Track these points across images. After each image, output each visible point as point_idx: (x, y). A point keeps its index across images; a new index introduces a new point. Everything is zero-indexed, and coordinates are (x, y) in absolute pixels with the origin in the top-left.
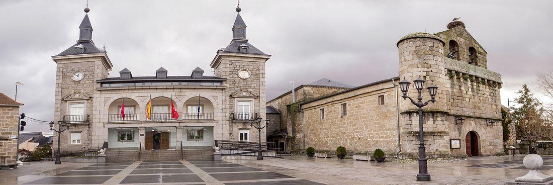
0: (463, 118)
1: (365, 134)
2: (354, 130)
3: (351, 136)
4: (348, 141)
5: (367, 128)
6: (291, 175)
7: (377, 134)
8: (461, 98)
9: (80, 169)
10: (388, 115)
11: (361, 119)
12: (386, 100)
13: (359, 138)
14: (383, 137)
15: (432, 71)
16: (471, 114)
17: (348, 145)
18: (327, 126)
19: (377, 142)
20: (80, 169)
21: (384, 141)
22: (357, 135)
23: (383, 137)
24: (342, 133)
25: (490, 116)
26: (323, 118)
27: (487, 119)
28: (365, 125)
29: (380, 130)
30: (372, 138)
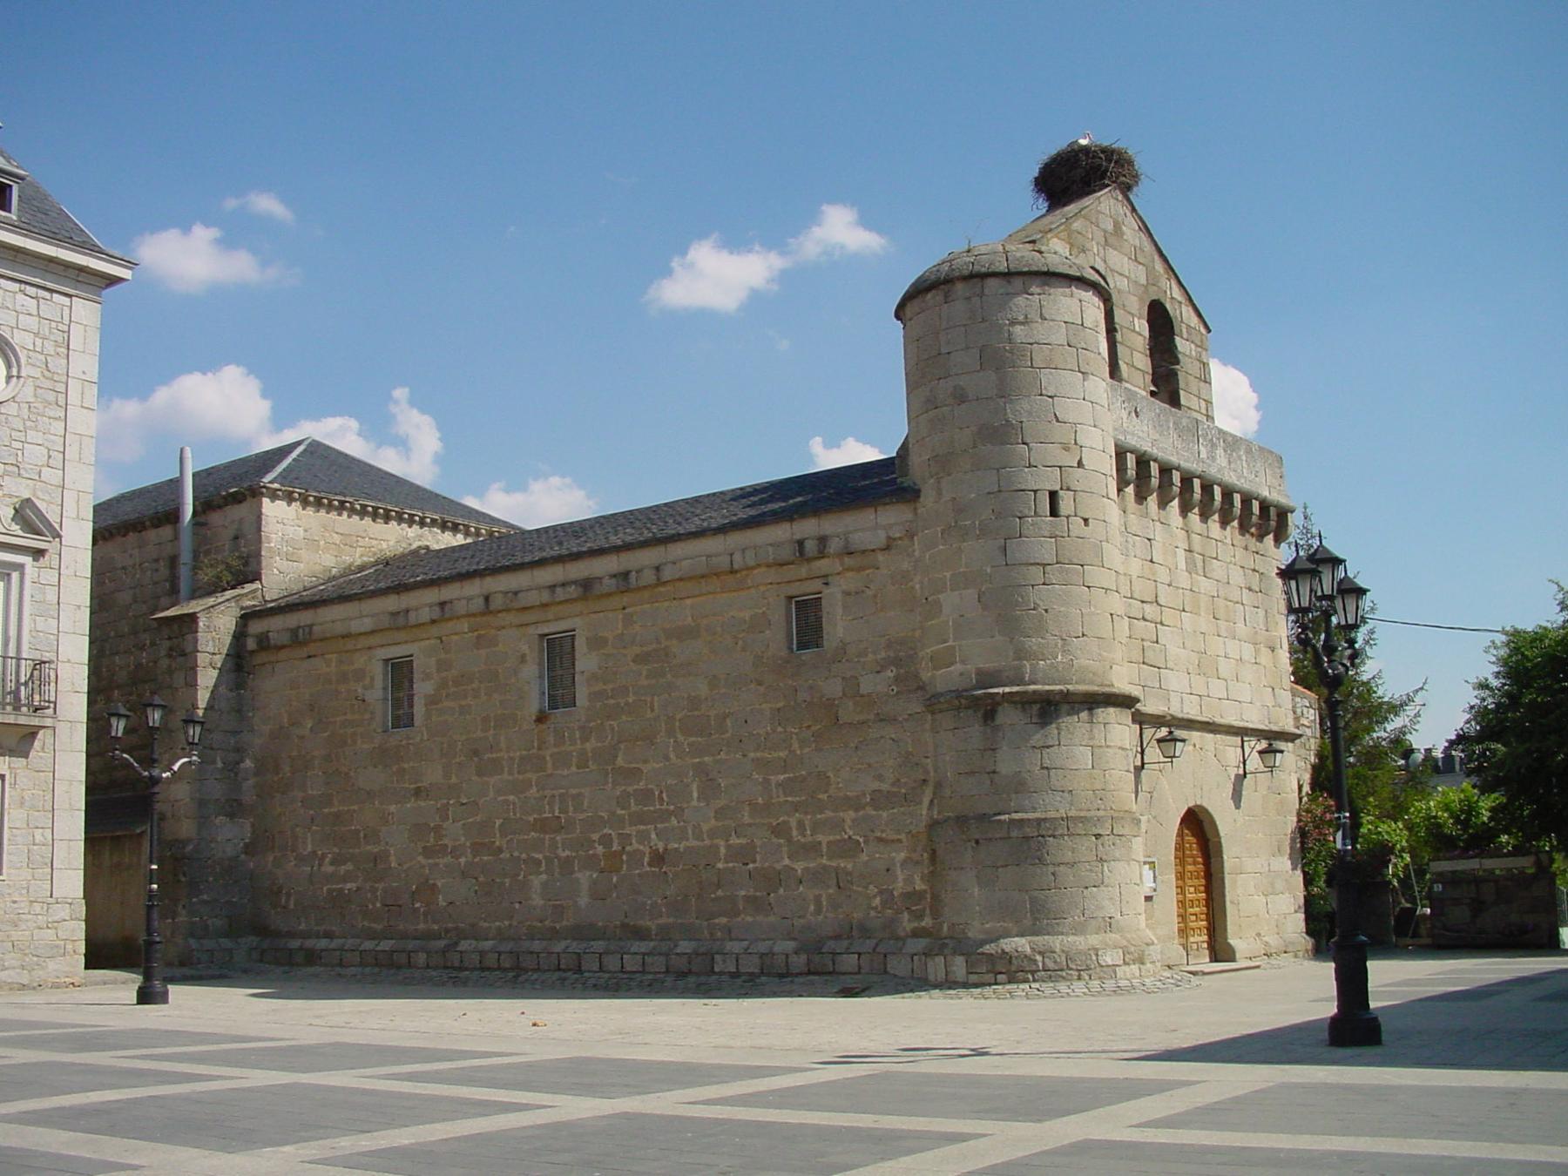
0: (1178, 733)
1: (699, 837)
2: (622, 801)
3: (606, 841)
4: (584, 878)
5: (710, 788)
6: (795, 1060)
7: (779, 831)
8: (1150, 610)
9: (1439, 974)
10: (848, 712)
11: (671, 733)
12: (837, 626)
13: (658, 858)
14: (813, 849)
15: (1080, 465)
16: (678, 584)
17: (583, 901)
18: (433, 774)
19: (773, 880)
20: (1439, 974)
21: (817, 876)
22: (643, 837)
23: (813, 849)
24: (543, 826)
25: (1254, 720)
26: (403, 720)
27: (1242, 732)
28: (701, 770)
29: (796, 807)
30: (744, 855)
